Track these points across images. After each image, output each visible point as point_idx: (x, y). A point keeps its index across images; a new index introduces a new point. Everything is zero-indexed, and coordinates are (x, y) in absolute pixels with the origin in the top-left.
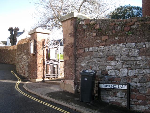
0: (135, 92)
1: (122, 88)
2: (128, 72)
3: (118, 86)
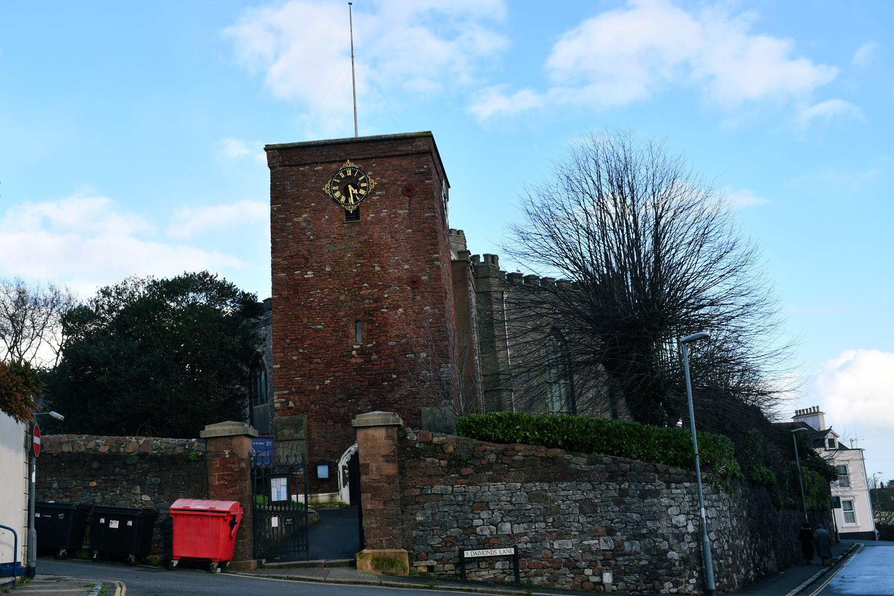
3: (498, 552)
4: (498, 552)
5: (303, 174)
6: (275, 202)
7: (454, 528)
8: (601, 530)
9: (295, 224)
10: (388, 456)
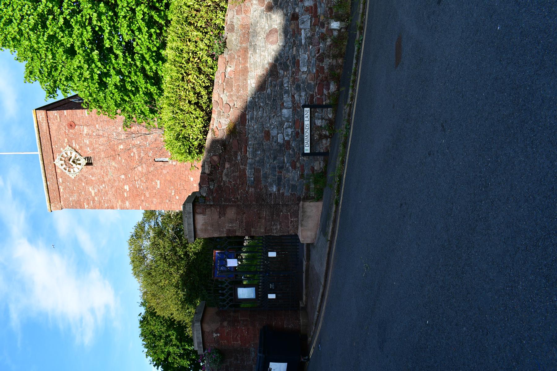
0: (314, 98)
1: (309, 115)
2: (286, 108)
3: (307, 122)
4: (307, 122)
5: (64, 189)
6: (82, 206)
7: (284, 160)
8: (293, 26)
9: (96, 195)
10: (220, 213)
